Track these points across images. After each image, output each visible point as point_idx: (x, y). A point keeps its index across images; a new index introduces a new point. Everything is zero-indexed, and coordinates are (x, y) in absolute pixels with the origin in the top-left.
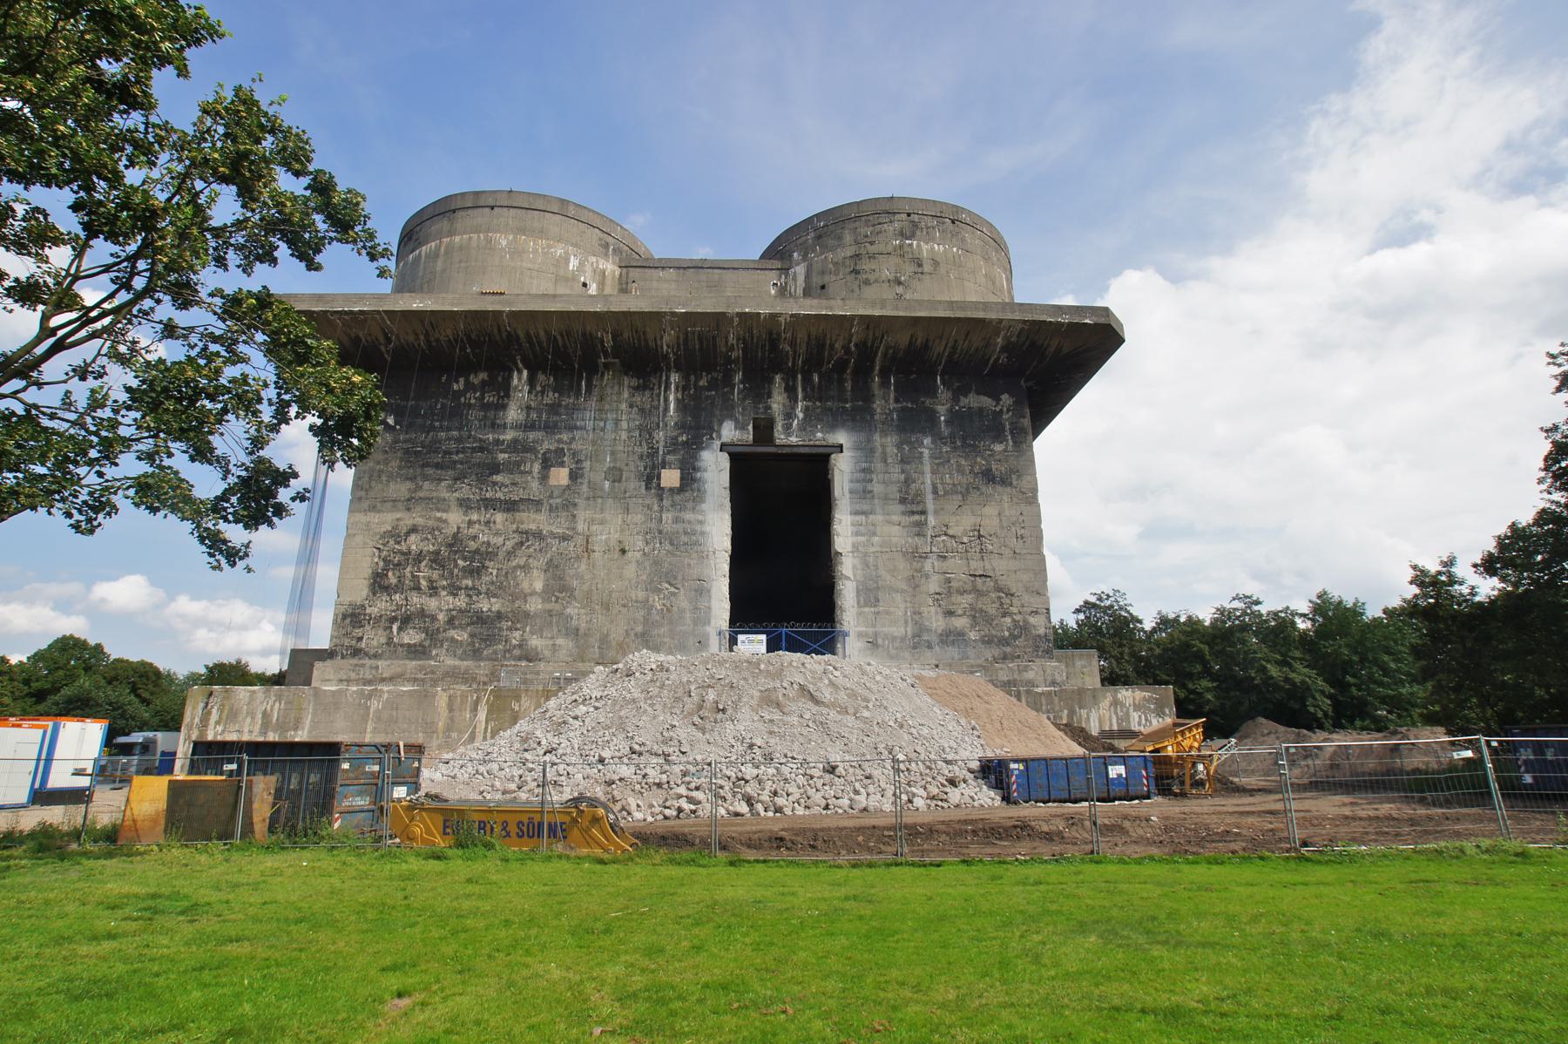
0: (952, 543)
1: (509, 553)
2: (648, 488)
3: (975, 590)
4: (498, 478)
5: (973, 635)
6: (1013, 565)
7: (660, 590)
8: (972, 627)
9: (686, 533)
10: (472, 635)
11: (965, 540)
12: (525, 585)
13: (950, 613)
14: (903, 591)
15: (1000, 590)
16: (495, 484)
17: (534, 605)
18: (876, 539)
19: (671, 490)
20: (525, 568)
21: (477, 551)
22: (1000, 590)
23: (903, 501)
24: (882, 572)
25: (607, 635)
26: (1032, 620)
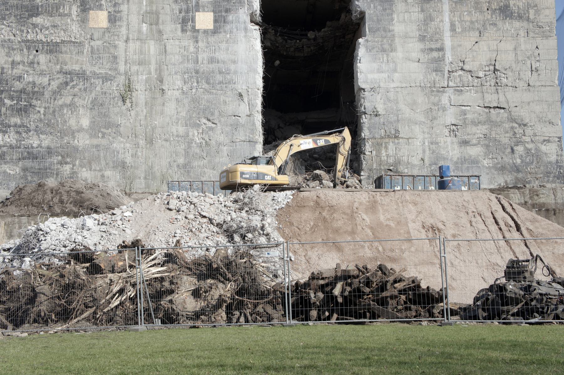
0: (467, 78)
1: (54, 93)
2: (183, 31)
3: (489, 121)
4: (38, 20)
5: (486, 162)
6: (527, 97)
7: (199, 126)
8: (486, 155)
9: (220, 72)
10: (25, 170)
11: (481, 74)
12: (72, 122)
13: (465, 143)
14: (421, 123)
15: (513, 120)
16: (35, 26)
17: (82, 141)
18: (396, 75)
19: (206, 32)
20: (72, 106)
21: (23, 91)
22: (513, 120)
23: (422, 39)
24: (402, 106)
25: (152, 167)
26: (543, 148)
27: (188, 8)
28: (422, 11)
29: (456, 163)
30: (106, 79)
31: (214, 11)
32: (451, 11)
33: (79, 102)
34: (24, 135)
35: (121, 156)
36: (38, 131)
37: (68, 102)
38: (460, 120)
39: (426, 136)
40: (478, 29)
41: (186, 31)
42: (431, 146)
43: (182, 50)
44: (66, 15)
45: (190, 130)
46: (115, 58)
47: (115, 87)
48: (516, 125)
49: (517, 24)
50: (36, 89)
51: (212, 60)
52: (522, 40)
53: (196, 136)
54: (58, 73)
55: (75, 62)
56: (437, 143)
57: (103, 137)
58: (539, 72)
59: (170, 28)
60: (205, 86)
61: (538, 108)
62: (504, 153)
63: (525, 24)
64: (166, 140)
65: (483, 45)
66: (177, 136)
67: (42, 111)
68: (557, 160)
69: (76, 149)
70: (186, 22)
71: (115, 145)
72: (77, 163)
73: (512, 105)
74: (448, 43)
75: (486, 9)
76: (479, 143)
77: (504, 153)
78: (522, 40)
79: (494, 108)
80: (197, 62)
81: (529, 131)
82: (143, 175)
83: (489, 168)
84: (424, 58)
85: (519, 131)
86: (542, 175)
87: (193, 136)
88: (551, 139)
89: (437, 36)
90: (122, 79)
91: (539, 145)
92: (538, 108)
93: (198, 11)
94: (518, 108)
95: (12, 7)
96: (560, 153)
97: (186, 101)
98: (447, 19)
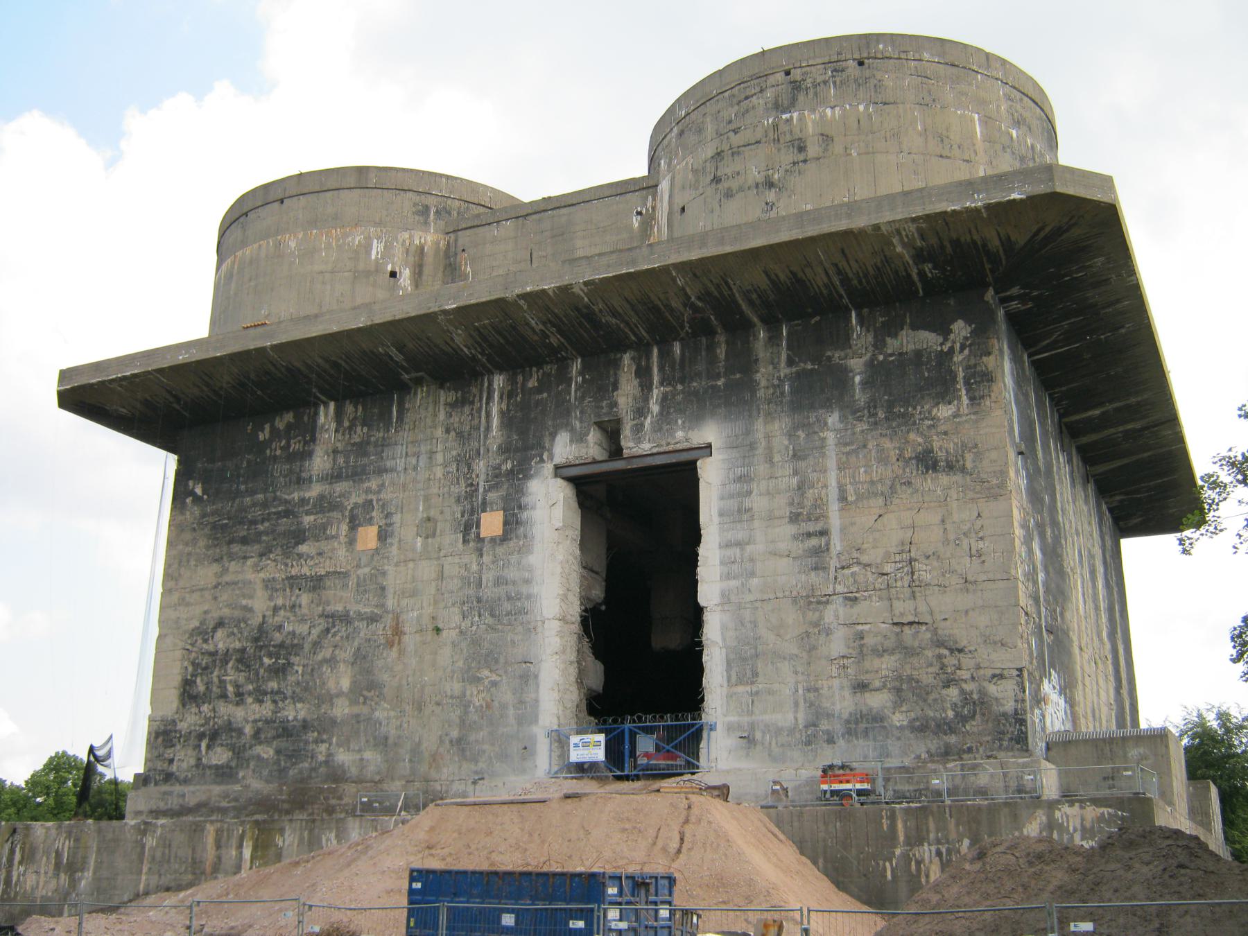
2: (465, 541)
4: (303, 548)
7: (479, 680)
8: (897, 706)
9: (509, 598)
10: (278, 752)
11: (889, 568)
14: (793, 657)
15: (940, 644)
16: (300, 556)
17: (341, 709)
18: (755, 581)
19: (493, 540)
21: (281, 645)
22: (940, 644)
23: (795, 518)
24: (762, 631)
26: (992, 689)
27: (472, 508)
28: (796, 473)
29: (848, 722)
30: (373, 619)
31: (505, 510)
32: (839, 469)
33: (341, 655)
34: (280, 704)
35: (383, 729)
36: (296, 698)
37: (328, 656)
38: (853, 648)
39: (801, 678)
40: (882, 493)
41: (468, 541)
42: (808, 695)
43: (462, 571)
44: (333, 537)
45: (468, 687)
46: (383, 589)
47: (380, 630)
48: (946, 652)
49: (944, 479)
50: (296, 641)
51: (499, 581)
52: (955, 505)
53: (477, 697)
54: (320, 616)
55: (340, 599)
56: (816, 690)
57: (364, 703)
58: (983, 558)
59: (450, 538)
60: (489, 620)
61: (982, 620)
62: (925, 701)
63: (958, 478)
64: (438, 704)
65: (891, 521)
66: (452, 697)
67: (300, 669)
68: (1016, 710)
69: (333, 722)
70: (469, 528)
71: (377, 714)
72: (334, 740)
73: (939, 617)
74: (835, 520)
75: (894, 459)
76: (884, 686)
77: (925, 701)
78: (955, 505)
79: (911, 623)
80: (479, 584)
81: (967, 661)
82: (407, 757)
83: (901, 728)
84: (799, 548)
85: (951, 661)
86: (989, 738)
87: (471, 695)
88: (1005, 672)
89: (818, 512)
90: (388, 620)
91: (986, 684)
92: (982, 620)
93: (484, 511)
94: (948, 623)
95: (279, 535)
96: (1020, 696)
97: (464, 645)
98: (832, 479)
